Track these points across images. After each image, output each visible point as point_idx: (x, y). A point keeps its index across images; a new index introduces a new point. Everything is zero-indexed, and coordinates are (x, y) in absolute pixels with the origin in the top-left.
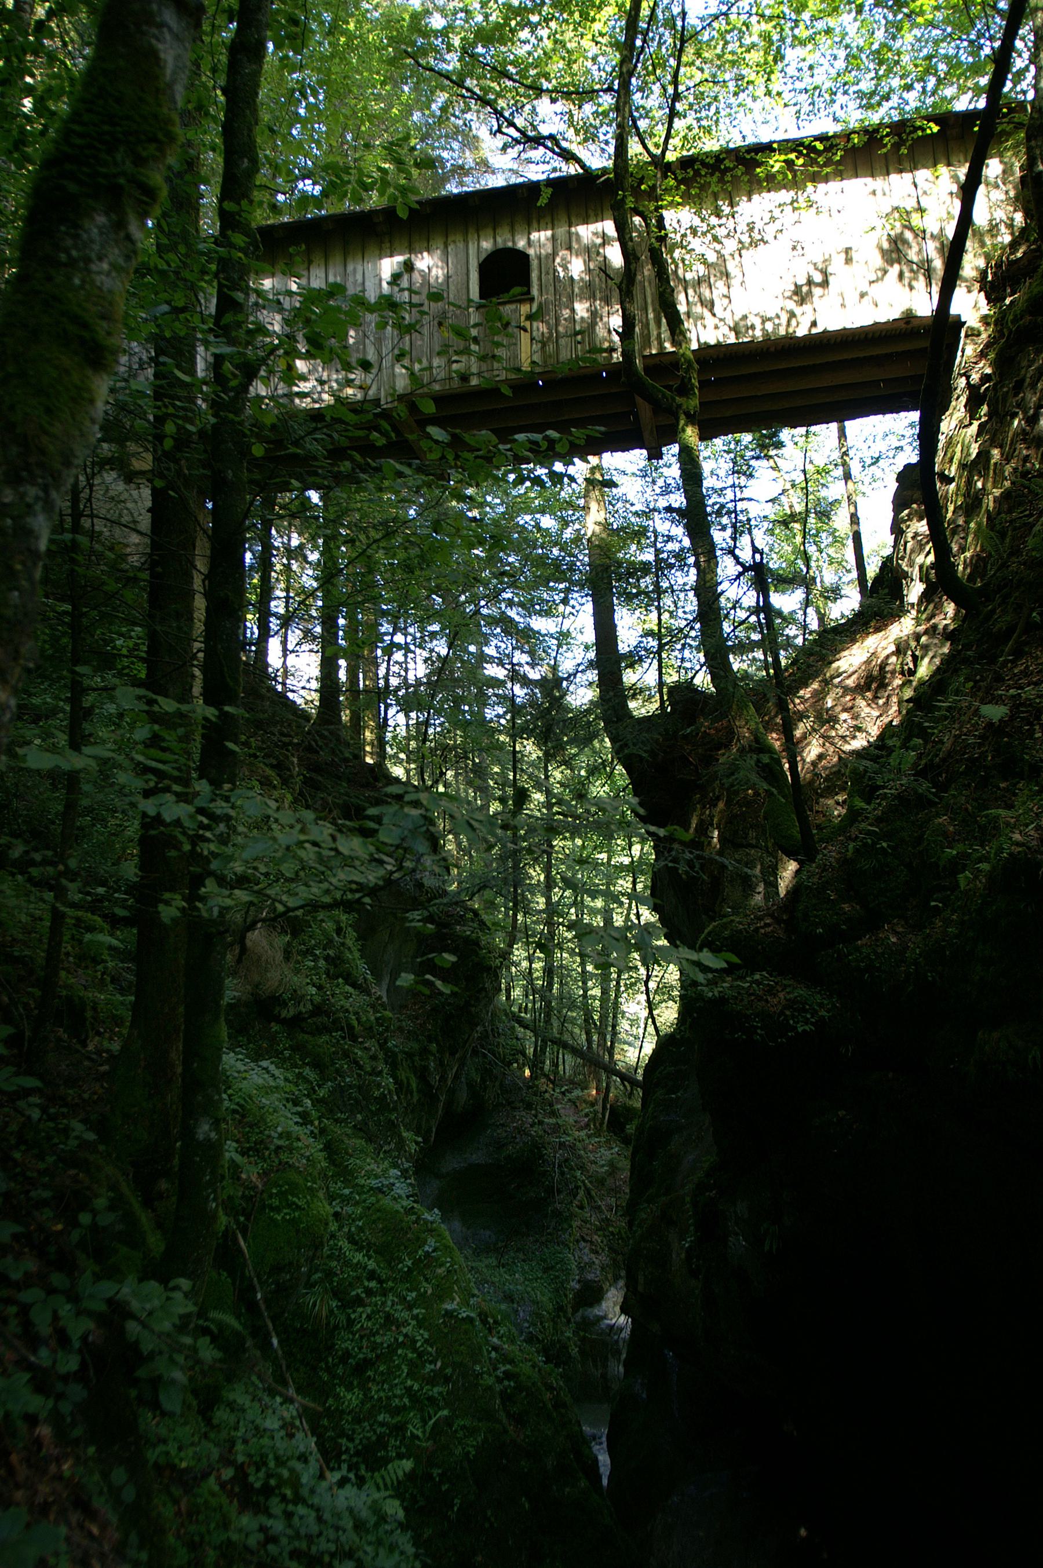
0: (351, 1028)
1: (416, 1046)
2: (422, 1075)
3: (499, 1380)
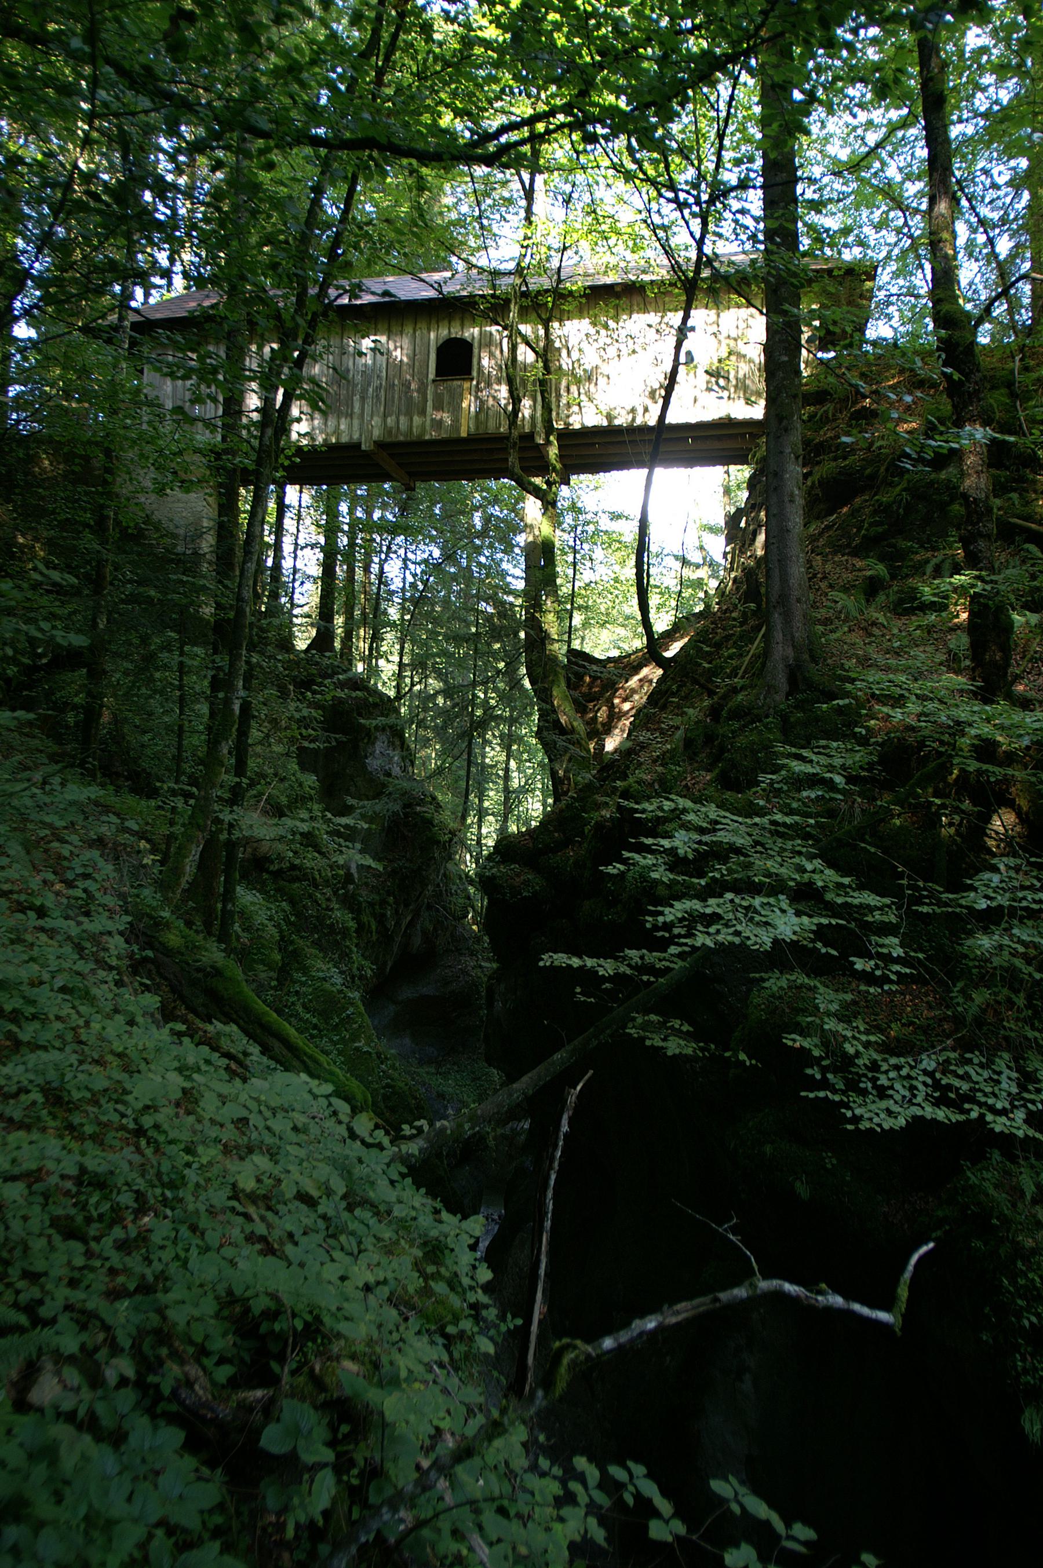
0: (314, 879)
1: (377, 898)
2: (381, 919)
3: (384, 1088)
